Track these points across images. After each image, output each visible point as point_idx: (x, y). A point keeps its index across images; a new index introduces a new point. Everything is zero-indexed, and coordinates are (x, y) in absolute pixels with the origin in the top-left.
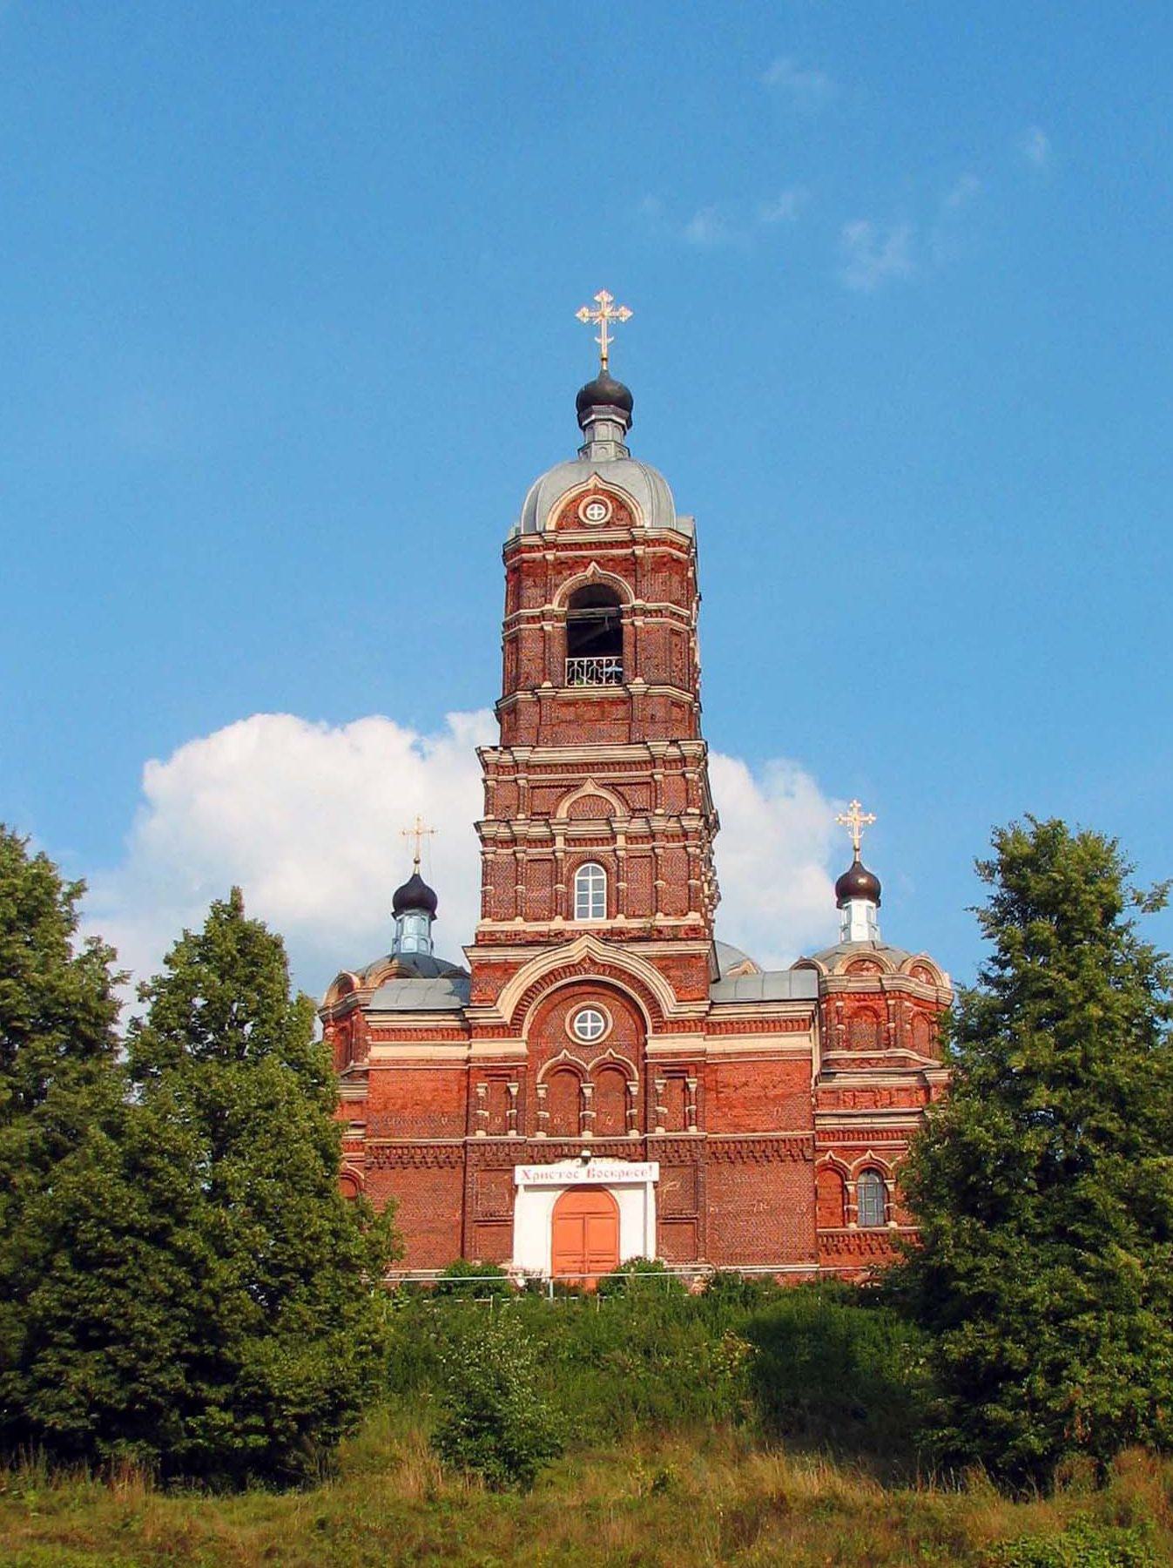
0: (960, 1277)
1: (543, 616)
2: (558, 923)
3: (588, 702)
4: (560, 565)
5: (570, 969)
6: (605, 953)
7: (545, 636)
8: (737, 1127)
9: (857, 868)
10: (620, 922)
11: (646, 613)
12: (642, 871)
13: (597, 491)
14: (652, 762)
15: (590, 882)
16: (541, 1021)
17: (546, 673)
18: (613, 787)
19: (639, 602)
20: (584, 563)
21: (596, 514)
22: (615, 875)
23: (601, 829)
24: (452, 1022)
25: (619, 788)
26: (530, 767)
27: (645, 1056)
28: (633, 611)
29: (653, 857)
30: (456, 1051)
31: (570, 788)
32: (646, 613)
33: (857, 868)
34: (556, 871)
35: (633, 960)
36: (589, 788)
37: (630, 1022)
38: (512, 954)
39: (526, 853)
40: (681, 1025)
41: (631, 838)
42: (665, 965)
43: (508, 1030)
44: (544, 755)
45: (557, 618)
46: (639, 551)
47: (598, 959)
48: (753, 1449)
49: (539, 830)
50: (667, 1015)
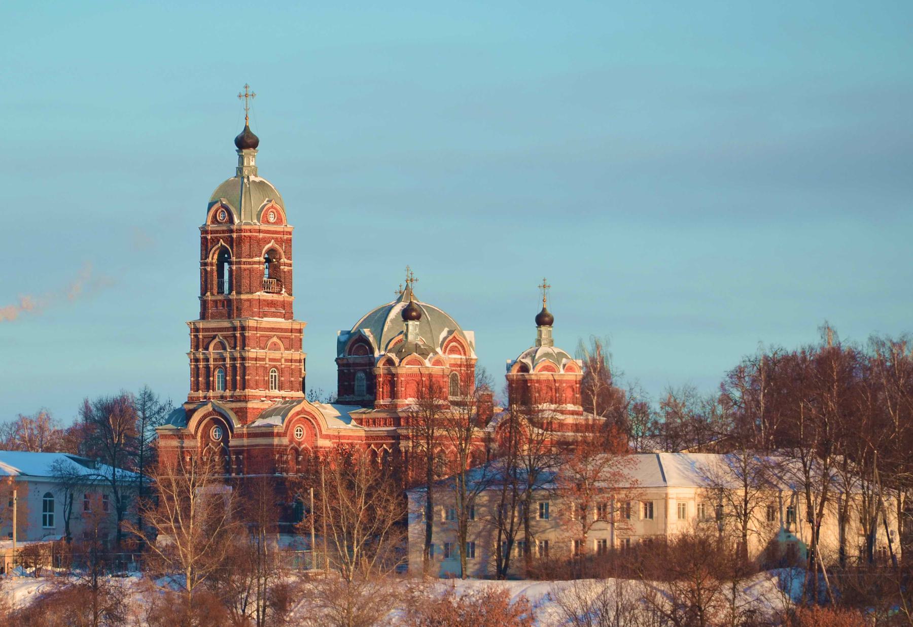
18: (280, 338)
25: (228, 339)
28: (285, 264)
31: (214, 337)
36: (275, 339)
41: (286, 360)
50: (324, 432)
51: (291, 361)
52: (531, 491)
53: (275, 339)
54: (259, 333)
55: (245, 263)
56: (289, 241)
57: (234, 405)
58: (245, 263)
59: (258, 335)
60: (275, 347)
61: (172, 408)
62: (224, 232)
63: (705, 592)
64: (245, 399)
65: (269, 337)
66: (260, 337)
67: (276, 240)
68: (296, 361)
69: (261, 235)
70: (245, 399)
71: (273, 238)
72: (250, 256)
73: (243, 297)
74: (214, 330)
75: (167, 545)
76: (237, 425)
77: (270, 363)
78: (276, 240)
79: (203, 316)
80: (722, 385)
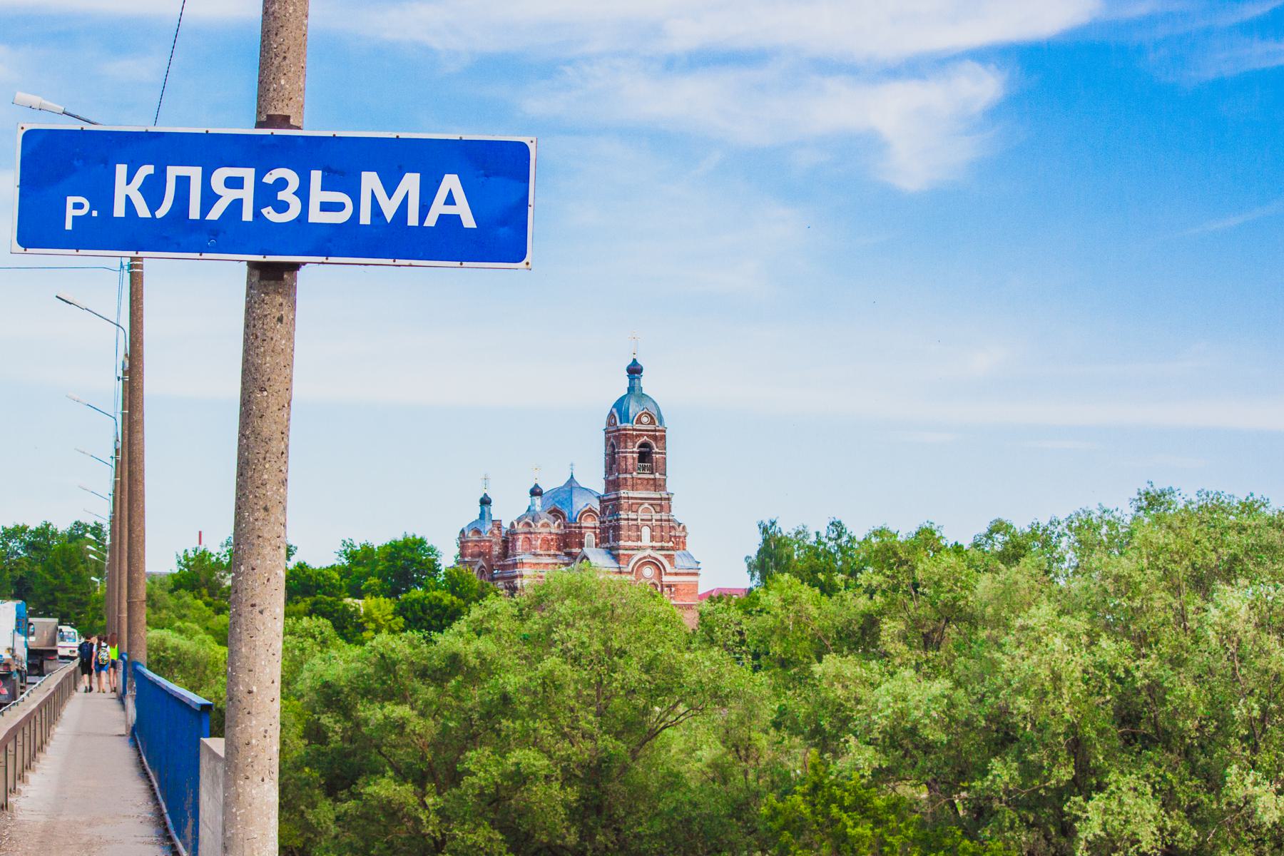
0: (461, 686)
1: (633, 452)
2: (639, 544)
3: (644, 479)
4: (637, 436)
5: (645, 558)
6: (654, 554)
7: (634, 459)
8: (682, 600)
9: (536, 486)
10: (654, 544)
11: (659, 453)
12: (658, 530)
13: (646, 413)
14: (661, 499)
15: (646, 532)
16: (637, 570)
17: (634, 470)
18: (651, 505)
19: (657, 450)
20: (642, 436)
21: (645, 419)
22: (652, 530)
23: (650, 517)
24: (617, 570)
26: (632, 498)
28: (656, 453)
29: (661, 526)
30: (617, 577)
31: (642, 504)
32: (659, 453)
33: (536, 486)
34: (638, 528)
35: (657, 554)
36: (646, 505)
37: (657, 572)
38: (630, 552)
39: (631, 523)
40: (670, 574)
41: (656, 520)
42: (666, 556)
43: (631, 573)
44: (631, 494)
45: (636, 453)
46: (657, 434)
48: (388, 768)
49: (635, 517)
51: (661, 520)
52: (898, 616)
53: (646, 505)
54: (630, 502)
55: (622, 452)
56: (664, 437)
57: (664, 552)
58: (622, 452)
61: (202, 548)
62: (652, 431)
63: (714, 662)
64: (618, 548)
67: (648, 436)
68: (665, 520)
70: (618, 548)
71: (646, 435)
72: (626, 448)
73: (621, 476)
74: (641, 499)
75: (1234, 716)
76: (669, 568)
78: (648, 436)
79: (607, 491)
80: (463, 532)
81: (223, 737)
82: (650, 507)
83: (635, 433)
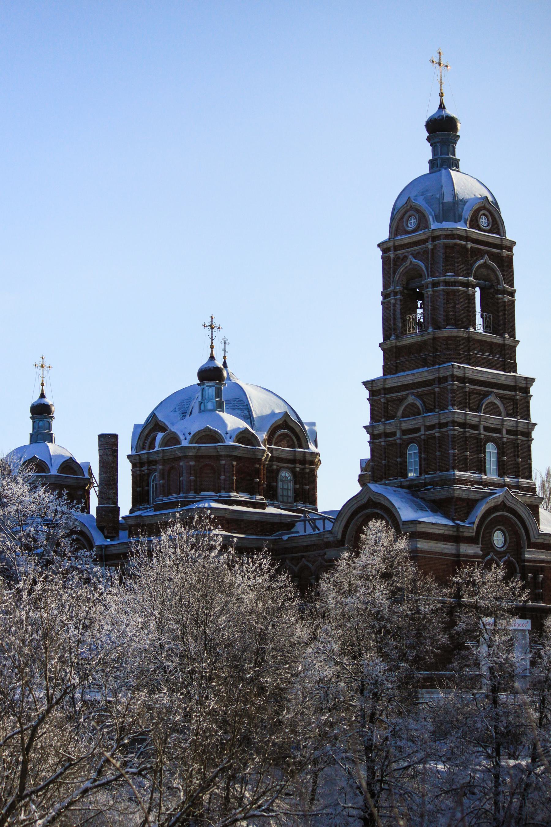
27: (524, 561)
30: (448, 548)
36: (491, 399)
47: (508, 504)
50: (533, 540)
59: (467, 389)
60: (493, 409)
65: (486, 395)
66: (470, 393)
69: (469, 245)
77: (509, 436)
81: (31, 442)
82: (497, 402)
83: (469, 245)
